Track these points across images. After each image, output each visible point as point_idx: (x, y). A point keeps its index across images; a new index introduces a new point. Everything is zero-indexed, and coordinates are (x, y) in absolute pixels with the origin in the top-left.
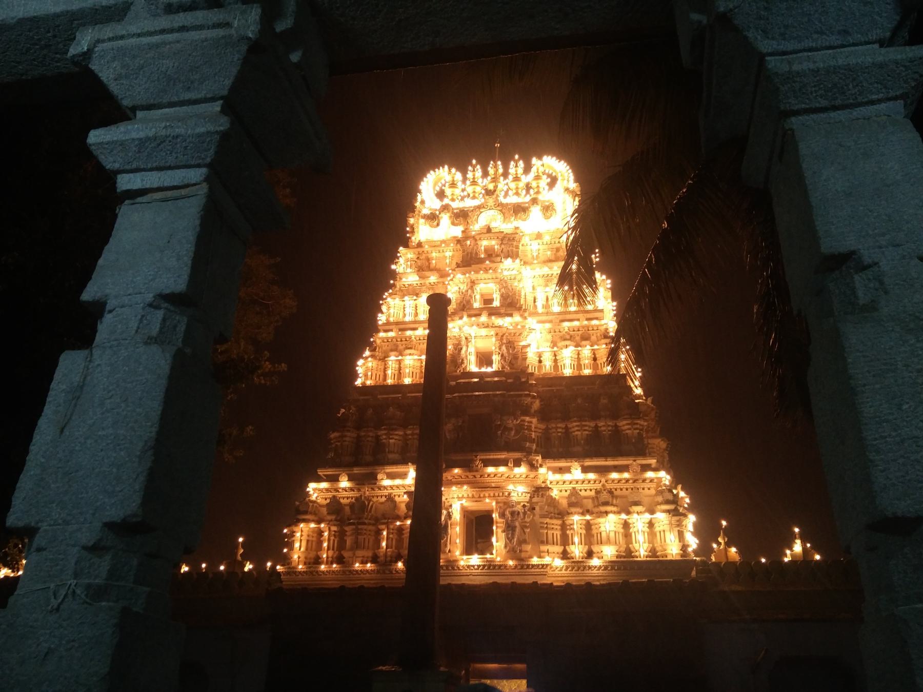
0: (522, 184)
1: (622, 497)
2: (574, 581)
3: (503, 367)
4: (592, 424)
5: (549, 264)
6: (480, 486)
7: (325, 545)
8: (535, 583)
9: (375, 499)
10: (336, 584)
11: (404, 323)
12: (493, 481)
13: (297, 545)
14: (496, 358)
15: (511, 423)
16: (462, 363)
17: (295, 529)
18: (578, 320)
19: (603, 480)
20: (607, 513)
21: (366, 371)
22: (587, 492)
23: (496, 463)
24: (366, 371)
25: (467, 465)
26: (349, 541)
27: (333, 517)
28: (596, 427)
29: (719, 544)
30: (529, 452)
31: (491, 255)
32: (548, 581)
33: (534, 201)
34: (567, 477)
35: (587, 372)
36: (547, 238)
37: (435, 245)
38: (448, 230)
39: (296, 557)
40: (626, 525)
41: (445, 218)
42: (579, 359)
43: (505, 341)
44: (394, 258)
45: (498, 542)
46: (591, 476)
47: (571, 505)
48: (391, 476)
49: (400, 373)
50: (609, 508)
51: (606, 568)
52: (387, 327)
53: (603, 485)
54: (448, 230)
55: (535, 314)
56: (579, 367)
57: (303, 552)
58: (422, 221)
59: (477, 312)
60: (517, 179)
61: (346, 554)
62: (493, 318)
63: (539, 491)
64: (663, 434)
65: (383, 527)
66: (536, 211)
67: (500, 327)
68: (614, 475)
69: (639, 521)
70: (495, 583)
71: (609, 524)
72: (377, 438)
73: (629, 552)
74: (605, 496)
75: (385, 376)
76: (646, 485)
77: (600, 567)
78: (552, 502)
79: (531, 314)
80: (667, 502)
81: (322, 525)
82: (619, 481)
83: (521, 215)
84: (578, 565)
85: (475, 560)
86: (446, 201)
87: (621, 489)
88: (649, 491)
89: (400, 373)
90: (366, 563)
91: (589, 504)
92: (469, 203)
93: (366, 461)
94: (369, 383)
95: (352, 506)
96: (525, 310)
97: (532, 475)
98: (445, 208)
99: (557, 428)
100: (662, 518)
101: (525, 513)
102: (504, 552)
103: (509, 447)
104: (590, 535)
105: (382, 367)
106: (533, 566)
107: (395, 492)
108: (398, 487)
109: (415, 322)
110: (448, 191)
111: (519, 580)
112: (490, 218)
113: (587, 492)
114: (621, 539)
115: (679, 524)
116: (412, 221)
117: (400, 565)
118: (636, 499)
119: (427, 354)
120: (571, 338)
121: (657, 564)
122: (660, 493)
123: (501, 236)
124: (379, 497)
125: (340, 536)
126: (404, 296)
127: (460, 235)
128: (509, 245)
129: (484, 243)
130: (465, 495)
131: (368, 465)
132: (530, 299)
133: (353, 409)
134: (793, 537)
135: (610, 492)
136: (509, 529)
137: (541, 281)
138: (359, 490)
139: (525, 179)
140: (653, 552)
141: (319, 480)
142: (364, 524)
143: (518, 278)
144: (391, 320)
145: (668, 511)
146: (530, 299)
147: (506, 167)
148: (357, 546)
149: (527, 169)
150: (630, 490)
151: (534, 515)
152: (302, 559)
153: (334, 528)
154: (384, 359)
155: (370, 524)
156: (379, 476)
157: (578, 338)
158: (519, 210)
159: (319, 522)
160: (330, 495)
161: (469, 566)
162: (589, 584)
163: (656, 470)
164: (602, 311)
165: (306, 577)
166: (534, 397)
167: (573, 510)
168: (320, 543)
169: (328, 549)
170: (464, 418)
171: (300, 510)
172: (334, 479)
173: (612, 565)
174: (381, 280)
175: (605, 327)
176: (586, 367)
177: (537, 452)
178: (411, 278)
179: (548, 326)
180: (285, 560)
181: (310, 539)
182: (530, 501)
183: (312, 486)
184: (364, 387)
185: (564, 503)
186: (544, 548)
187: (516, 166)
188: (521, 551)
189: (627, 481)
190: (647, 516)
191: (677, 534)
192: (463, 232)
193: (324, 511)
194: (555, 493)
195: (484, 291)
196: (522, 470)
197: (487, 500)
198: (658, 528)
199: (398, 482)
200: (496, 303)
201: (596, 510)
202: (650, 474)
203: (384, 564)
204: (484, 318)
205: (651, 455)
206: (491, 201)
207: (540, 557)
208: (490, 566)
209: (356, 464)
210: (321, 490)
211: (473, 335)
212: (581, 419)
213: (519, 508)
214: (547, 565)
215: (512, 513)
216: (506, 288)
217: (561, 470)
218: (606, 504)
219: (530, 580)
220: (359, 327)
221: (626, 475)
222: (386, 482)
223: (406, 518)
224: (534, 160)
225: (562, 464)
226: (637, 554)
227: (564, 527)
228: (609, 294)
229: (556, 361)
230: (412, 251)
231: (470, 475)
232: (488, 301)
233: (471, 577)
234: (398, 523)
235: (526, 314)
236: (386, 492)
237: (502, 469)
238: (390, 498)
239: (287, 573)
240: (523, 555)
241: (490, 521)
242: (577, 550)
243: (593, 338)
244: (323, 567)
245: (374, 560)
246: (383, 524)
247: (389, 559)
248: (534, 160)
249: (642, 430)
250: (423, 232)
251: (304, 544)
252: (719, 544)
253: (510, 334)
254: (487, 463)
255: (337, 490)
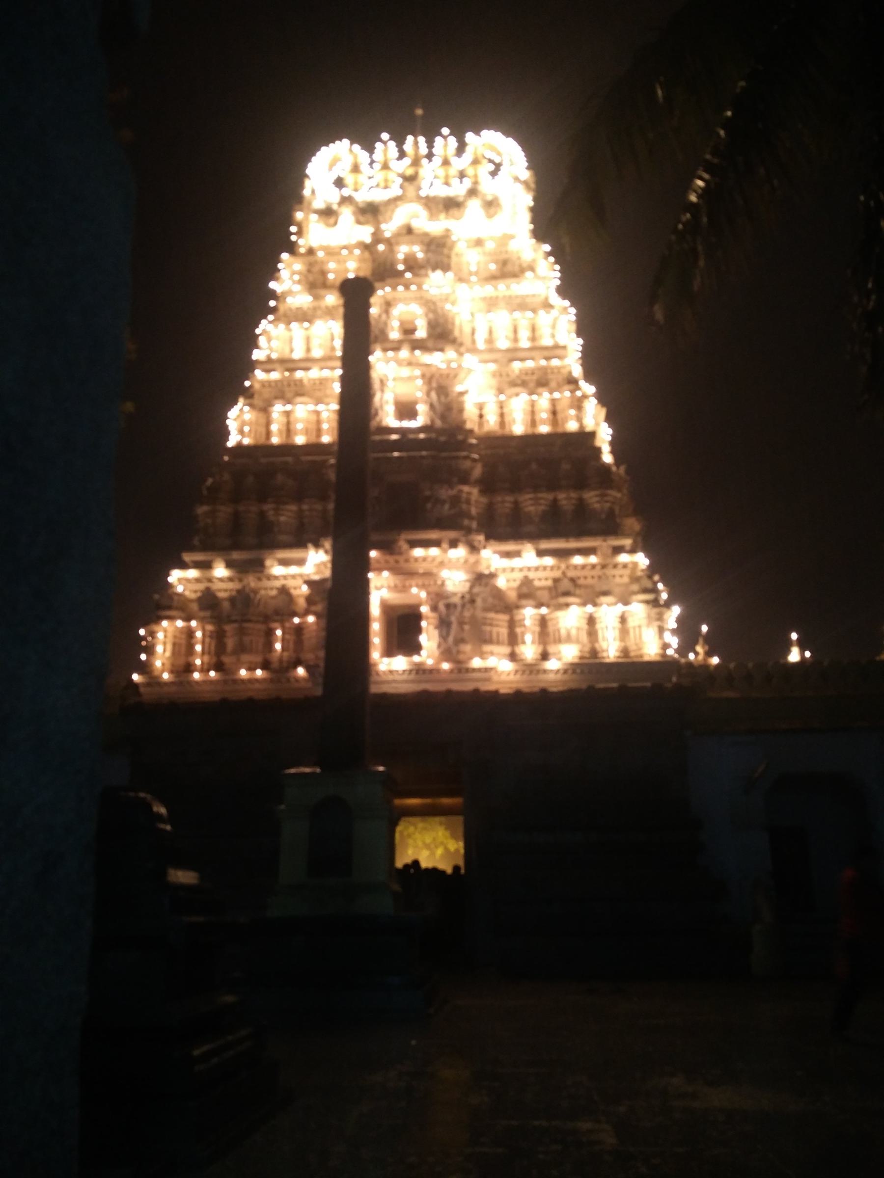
0: (453, 171)
1: (586, 587)
2: (525, 687)
3: (432, 421)
4: (550, 496)
5: (493, 282)
6: (405, 573)
7: (198, 648)
8: (476, 691)
9: (263, 592)
10: (217, 697)
11: (293, 361)
12: (421, 568)
13: (159, 649)
14: (422, 409)
15: (445, 493)
16: (376, 414)
17: (155, 628)
18: (533, 359)
19: (563, 566)
20: (567, 605)
21: (240, 425)
22: (542, 580)
23: (426, 544)
24: (240, 425)
25: (387, 547)
26: (230, 643)
27: (208, 614)
28: (555, 500)
29: (696, 654)
30: (469, 531)
31: (412, 264)
32: (491, 687)
33: (473, 192)
34: (516, 562)
35: (544, 429)
36: (490, 246)
37: (332, 253)
38: (350, 231)
39: (158, 664)
40: (591, 621)
41: (347, 214)
42: (533, 413)
43: (434, 385)
44: (273, 272)
45: (429, 640)
46: (549, 561)
47: (522, 596)
48: (285, 563)
49: (289, 430)
50: (570, 599)
51: (565, 672)
52: (269, 367)
53: (564, 573)
54: (350, 231)
55: (474, 350)
56: (533, 423)
57: (169, 658)
58: (314, 217)
59: (395, 345)
60: (446, 163)
61: (227, 660)
62: (417, 352)
63: (482, 579)
64: (638, 511)
65: (276, 625)
66: (474, 206)
67: (427, 365)
68: (578, 560)
69: (608, 614)
70: (425, 692)
71: (571, 618)
72: (262, 514)
73: (594, 653)
74: (566, 585)
75: (268, 434)
76: (617, 572)
77: (558, 671)
78: (498, 594)
79: (469, 351)
80: (645, 591)
81: (194, 623)
82: (584, 567)
83: (454, 212)
84: (531, 669)
85: (400, 663)
86: (346, 192)
87: (585, 578)
88: (621, 578)
89: (289, 430)
90: (255, 669)
91: (544, 596)
92: (379, 196)
93: (250, 542)
94: (246, 441)
95: (232, 600)
96: (461, 344)
97: (472, 559)
98: (346, 200)
99: (503, 502)
100: (638, 610)
101: (463, 606)
102: (436, 653)
103: (442, 524)
104: (545, 632)
105: (263, 420)
106: (474, 670)
107: (290, 583)
108: (293, 577)
109: (308, 360)
110: (349, 179)
111: (456, 687)
112: (410, 214)
113: (542, 580)
114: (584, 638)
115: (660, 618)
116: (299, 215)
117: (301, 671)
118: (605, 588)
119: (344, 366)
120: (524, 384)
121: (631, 668)
122: (635, 579)
123: (427, 240)
124: (268, 590)
125: (218, 639)
126: (288, 323)
127: (368, 240)
128: (439, 253)
129: (402, 251)
130: (386, 585)
131: (249, 548)
132: (467, 330)
133: (226, 477)
134: (788, 644)
135: (573, 580)
136: (443, 625)
137: (482, 305)
138: (240, 580)
139: (459, 164)
140: (625, 652)
141: (184, 566)
142: (250, 621)
143: (452, 298)
144: (274, 356)
145: (647, 602)
146: (467, 330)
147: (430, 144)
148: (241, 649)
149: (461, 148)
150: (596, 579)
151: (475, 608)
152: (168, 666)
153: (210, 628)
154: (265, 410)
155: (257, 622)
156: (268, 563)
157: (532, 385)
158: (451, 205)
159: (188, 619)
160: (201, 586)
161: (391, 672)
162: (544, 691)
163: (633, 551)
164: (564, 347)
165: (174, 689)
166: (475, 460)
167: (524, 602)
168: (190, 648)
169: (203, 652)
170: (384, 485)
171: (163, 604)
172: (206, 566)
173: (573, 668)
174: (255, 303)
175: (567, 370)
176: (543, 422)
177: (478, 531)
178: (300, 299)
179: (493, 367)
180: (145, 668)
181: (177, 640)
182: (470, 592)
183: (175, 576)
184: (239, 447)
185: (512, 595)
186: (487, 648)
187: (446, 145)
188: (458, 652)
189: (593, 566)
190: (620, 608)
191: (656, 629)
192: (374, 234)
193: (195, 607)
194: (501, 583)
195: (406, 317)
196: (460, 553)
197: (414, 590)
198: (632, 623)
199: (293, 570)
200: (421, 333)
201: (554, 602)
202: (623, 558)
203: (280, 670)
204: (404, 353)
205: (625, 535)
206: (411, 189)
207: (482, 658)
208: (419, 670)
209: (236, 546)
210: (188, 580)
211: (391, 377)
212: (536, 488)
213: (456, 600)
214: (491, 669)
215: (448, 606)
216: (435, 311)
217: (508, 555)
218: (567, 594)
219: (468, 687)
220: (226, 368)
221: (593, 559)
222: (277, 570)
223: (307, 612)
224: (470, 137)
225: (510, 547)
226: (605, 654)
227: (512, 625)
228: (573, 327)
229: (502, 415)
230: (300, 260)
231: (391, 559)
232: (408, 330)
233: (394, 685)
234: (296, 620)
235: (462, 349)
236: (278, 584)
237: (434, 551)
238: (284, 591)
239: (148, 685)
240: (461, 657)
241: (418, 617)
242: (529, 651)
243: (553, 384)
244: (196, 676)
245: (265, 666)
246: (276, 621)
247: (285, 665)
248: (470, 137)
249: (613, 503)
250: (313, 234)
251: (169, 647)
252: (696, 654)
253: (441, 375)
254: (414, 544)
255: (210, 580)
